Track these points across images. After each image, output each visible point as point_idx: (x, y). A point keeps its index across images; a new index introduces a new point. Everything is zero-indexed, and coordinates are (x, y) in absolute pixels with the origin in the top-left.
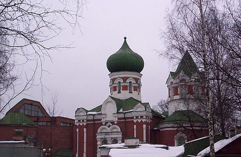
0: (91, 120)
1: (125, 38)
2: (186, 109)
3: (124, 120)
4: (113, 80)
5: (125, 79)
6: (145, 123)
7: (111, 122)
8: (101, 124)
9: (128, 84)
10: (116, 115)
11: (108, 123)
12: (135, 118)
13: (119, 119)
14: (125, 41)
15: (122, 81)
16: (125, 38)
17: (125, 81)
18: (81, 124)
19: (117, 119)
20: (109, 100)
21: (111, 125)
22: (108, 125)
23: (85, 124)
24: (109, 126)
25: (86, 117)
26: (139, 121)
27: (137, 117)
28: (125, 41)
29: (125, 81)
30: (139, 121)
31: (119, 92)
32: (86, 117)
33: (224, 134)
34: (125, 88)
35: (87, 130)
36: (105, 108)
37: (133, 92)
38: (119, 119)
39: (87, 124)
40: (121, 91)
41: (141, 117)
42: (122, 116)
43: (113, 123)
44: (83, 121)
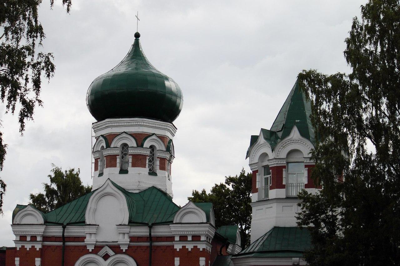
0: (55, 239)
1: (137, 36)
2: (315, 164)
3: (147, 244)
4: (108, 139)
5: (140, 138)
6: (204, 253)
7: (111, 247)
8: (84, 250)
9: (148, 153)
10: (127, 230)
11: (101, 247)
12: (177, 239)
13: (132, 239)
14: (136, 45)
15: (132, 143)
16: (137, 36)
17: (140, 145)
18: (28, 246)
19: (126, 240)
20: (109, 190)
21: (111, 252)
22: (102, 252)
23: (38, 247)
24: (106, 257)
25: (41, 229)
26: (190, 247)
27: (183, 238)
28: (136, 45)
29: (140, 145)
30: (190, 247)
31: (123, 171)
32: (41, 229)
33: (137, 247)
34: (138, 161)
35: (20, 260)
36: (95, 210)
37: (158, 171)
38: (132, 239)
39: (43, 246)
40: (130, 169)
41: (180, 237)
42: (142, 231)
43: (116, 249)
44: (34, 238)
